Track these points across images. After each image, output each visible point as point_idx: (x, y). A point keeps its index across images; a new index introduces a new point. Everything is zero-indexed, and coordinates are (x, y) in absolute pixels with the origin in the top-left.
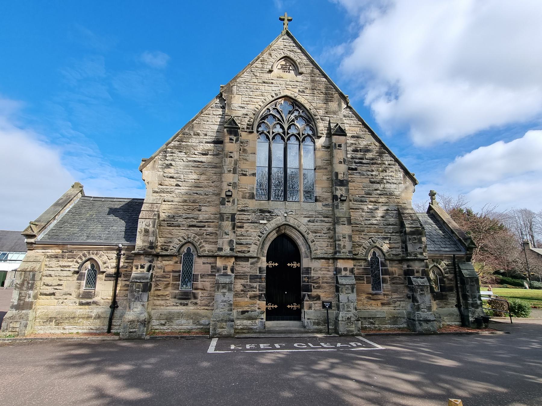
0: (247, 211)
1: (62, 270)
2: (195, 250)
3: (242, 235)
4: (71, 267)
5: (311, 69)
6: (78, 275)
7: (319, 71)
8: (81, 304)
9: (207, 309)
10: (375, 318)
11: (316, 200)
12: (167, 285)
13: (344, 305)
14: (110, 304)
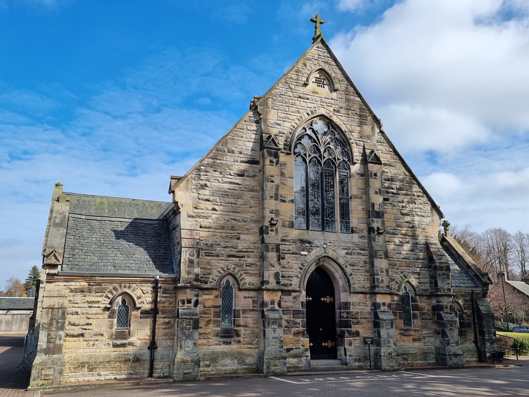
0: (287, 241)
1: (90, 307)
2: (235, 282)
3: (284, 266)
4: (100, 303)
5: (346, 86)
6: (109, 312)
7: (354, 89)
8: (115, 346)
9: (250, 348)
10: (408, 354)
11: (353, 232)
12: (208, 322)
13: (384, 340)
14: (149, 345)
